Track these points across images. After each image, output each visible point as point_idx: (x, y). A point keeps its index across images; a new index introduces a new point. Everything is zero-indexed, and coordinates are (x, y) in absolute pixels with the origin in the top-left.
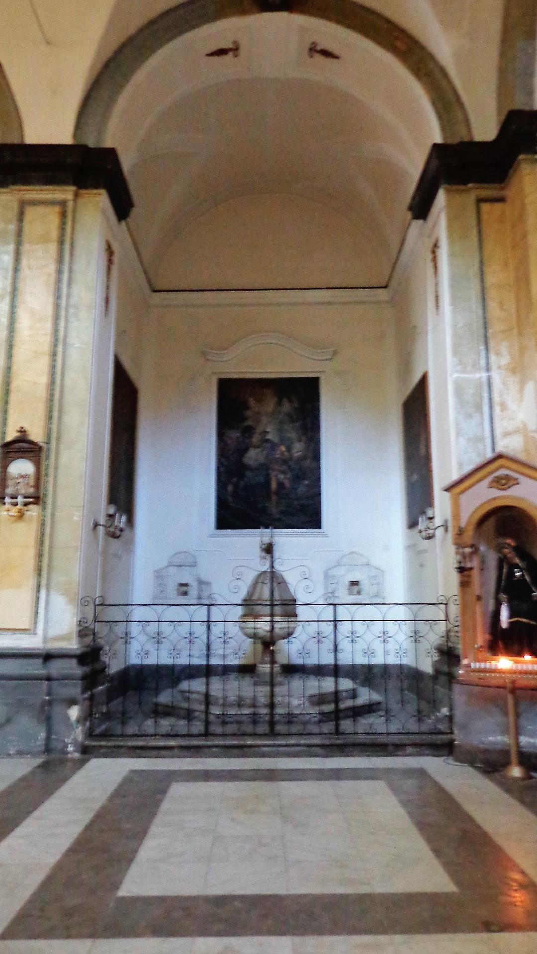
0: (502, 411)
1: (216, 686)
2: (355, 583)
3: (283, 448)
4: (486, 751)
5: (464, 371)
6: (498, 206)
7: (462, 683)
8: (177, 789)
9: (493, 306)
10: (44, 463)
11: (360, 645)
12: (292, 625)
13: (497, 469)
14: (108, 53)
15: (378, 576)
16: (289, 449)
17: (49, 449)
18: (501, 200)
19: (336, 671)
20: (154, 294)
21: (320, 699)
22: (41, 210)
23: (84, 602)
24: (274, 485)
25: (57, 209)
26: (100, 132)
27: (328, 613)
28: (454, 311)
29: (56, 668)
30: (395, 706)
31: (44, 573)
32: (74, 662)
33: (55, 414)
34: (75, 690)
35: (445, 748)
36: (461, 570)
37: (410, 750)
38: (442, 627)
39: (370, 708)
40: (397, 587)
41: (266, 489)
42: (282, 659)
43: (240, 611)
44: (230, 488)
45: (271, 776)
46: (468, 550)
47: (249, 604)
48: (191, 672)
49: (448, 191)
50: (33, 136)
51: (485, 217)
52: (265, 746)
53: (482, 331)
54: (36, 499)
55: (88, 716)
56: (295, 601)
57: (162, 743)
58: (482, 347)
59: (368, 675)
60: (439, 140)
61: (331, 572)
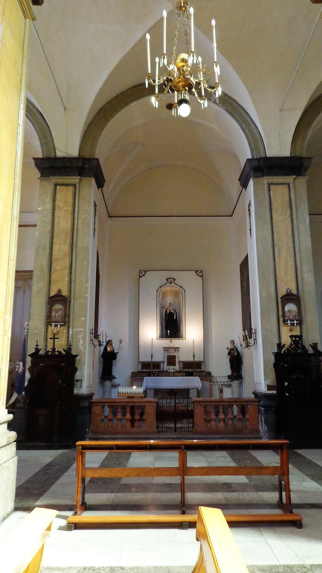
17: (70, 299)
22: (279, 187)
50: (271, 153)
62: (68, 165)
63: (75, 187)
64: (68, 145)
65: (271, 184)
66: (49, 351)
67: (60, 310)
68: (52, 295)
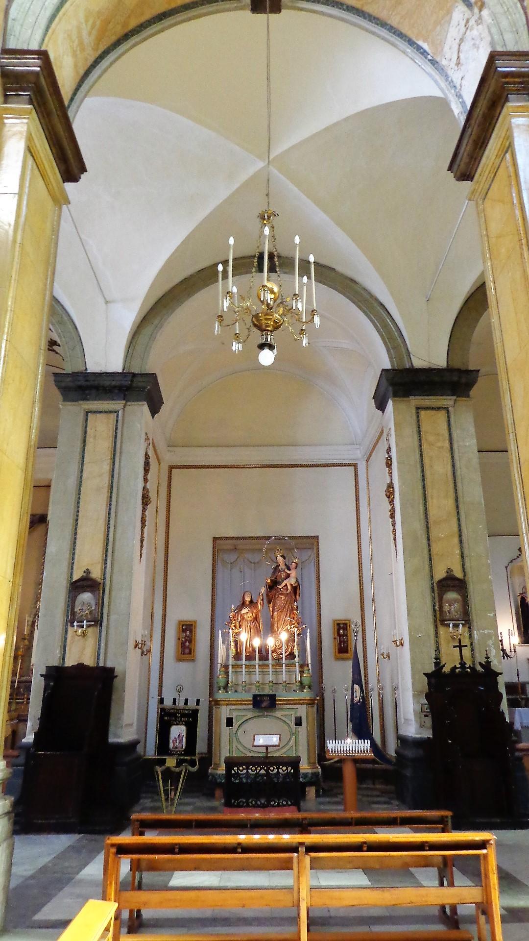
17: (104, 583)
50: (93, 366)
54: (97, 621)
62: (437, 379)
63: (448, 412)
64: (106, 355)
65: (90, 412)
66: (455, 668)
67: (456, 600)
68: (75, 578)
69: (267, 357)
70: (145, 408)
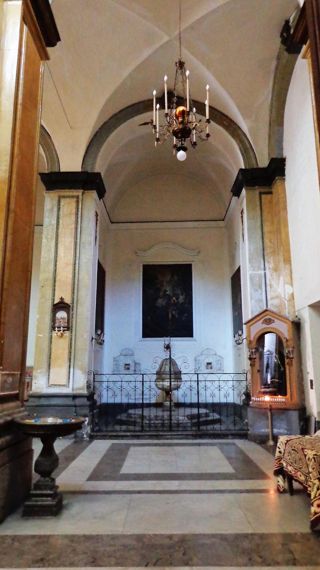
0: (271, 288)
1: (146, 412)
2: (210, 364)
3: (174, 298)
4: (261, 436)
5: (254, 270)
6: (269, 196)
7: (252, 407)
8: (132, 449)
9: (267, 241)
10: (71, 312)
11: (209, 392)
12: (179, 383)
13: (266, 315)
14: (97, 129)
15: (220, 359)
16: (177, 299)
17: (73, 306)
18: (271, 193)
19: (198, 405)
20: (112, 224)
21: (191, 417)
22: (68, 200)
23: (89, 373)
24: (170, 316)
25: (75, 199)
26: (94, 164)
27: (195, 378)
28: (249, 244)
29: (78, 402)
30: (224, 419)
31: (72, 361)
32: (85, 399)
33: (76, 291)
34: (86, 411)
35: (244, 436)
36: (250, 359)
37: (230, 437)
38: (244, 384)
39: (214, 422)
40: (229, 366)
41: (168, 312)
42: (175, 400)
43: (155, 377)
44: (149, 318)
45: (170, 445)
46: (254, 350)
47: (159, 373)
48: (135, 406)
49: (246, 189)
51: (263, 200)
52: (168, 435)
53: (262, 253)
54: (68, 328)
55: (91, 422)
56: (181, 372)
57: (124, 434)
58: (262, 260)
59: (215, 407)
60: (243, 168)
61: (198, 358)
68: (55, 303)
69: (181, 155)
70: (94, 194)
